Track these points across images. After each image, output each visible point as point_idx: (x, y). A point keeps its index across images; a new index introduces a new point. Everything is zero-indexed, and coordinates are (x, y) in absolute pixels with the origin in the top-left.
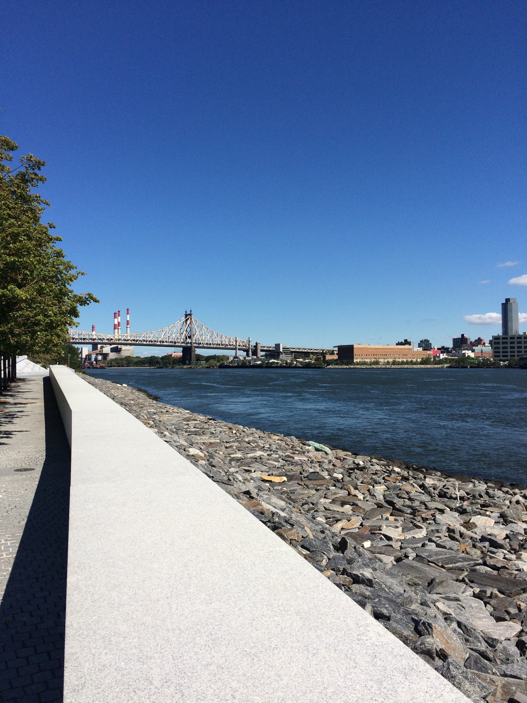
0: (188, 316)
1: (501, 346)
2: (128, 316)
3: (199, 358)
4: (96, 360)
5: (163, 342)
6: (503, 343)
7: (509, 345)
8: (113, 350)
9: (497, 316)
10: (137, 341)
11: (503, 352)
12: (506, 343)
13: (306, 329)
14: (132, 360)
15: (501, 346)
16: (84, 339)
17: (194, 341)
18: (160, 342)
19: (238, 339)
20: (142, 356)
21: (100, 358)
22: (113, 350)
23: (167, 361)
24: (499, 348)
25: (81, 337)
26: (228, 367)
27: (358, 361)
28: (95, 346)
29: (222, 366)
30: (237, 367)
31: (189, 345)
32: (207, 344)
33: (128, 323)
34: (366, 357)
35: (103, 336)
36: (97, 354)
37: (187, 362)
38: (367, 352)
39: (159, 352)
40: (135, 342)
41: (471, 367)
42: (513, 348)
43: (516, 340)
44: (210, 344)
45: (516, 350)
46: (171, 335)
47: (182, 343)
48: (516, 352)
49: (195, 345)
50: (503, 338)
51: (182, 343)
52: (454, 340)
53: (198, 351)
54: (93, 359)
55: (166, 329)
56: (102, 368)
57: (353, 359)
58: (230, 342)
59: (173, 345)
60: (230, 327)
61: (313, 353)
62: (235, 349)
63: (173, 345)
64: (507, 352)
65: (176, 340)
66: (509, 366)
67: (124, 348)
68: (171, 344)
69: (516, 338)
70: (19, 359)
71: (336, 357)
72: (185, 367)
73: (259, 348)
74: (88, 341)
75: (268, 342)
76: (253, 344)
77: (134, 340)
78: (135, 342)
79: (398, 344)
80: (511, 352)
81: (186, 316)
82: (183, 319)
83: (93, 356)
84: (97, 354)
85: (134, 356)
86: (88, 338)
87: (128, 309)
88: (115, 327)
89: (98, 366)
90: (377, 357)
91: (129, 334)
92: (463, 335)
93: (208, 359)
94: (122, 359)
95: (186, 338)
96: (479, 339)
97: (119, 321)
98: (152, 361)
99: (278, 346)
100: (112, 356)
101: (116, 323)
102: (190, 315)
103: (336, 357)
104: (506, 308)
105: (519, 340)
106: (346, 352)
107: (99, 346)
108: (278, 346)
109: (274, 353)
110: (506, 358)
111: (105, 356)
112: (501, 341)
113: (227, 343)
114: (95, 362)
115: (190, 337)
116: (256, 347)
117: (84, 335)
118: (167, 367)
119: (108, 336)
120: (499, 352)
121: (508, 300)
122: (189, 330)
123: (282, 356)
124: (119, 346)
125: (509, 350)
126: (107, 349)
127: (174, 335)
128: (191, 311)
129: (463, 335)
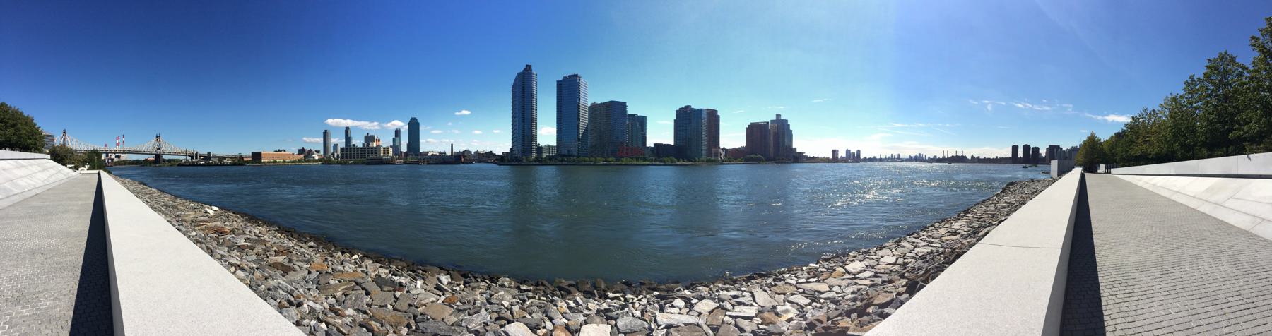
9: (321, 140)
39: (142, 157)
53: (164, 157)
60: (183, 141)
66: (354, 163)
70: (554, 143)
75: (203, 151)
91: (124, 148)
92: (778, 116)
93: (169, 161)
98: (137, 162)
104: (325, 134)
106: (257, 156)
109: (208, 157)
129: (778, 116)
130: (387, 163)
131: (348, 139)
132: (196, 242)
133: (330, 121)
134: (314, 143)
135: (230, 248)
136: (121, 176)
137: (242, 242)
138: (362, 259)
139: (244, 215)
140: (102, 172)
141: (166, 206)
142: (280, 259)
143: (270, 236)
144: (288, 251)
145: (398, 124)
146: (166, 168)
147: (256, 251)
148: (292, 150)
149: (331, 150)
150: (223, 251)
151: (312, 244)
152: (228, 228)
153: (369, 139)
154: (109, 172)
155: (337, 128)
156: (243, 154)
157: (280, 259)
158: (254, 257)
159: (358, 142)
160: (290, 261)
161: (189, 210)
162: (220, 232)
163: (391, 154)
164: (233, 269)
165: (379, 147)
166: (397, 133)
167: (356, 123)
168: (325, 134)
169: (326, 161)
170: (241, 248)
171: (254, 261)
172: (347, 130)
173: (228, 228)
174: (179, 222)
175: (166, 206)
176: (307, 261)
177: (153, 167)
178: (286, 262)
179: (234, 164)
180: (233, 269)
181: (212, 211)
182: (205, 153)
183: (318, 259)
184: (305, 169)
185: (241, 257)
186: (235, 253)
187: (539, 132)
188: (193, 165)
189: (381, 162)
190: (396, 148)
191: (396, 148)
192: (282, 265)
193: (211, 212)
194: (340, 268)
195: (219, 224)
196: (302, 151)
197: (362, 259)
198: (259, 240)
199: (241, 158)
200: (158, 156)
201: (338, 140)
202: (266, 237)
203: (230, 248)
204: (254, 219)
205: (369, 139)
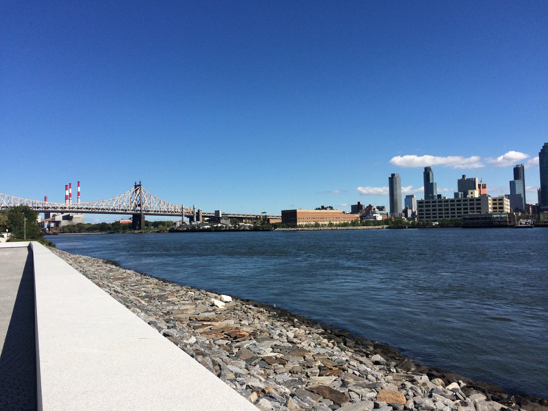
0: (137, 186)
1: (424, 209)
2: (79, 188)
3: (147, 224)
4: (49, 227)
5: (115, 210)
6: (426, 206)
7: (431, 208)
8: (65, 218)
9: (386, 190)
10: (90, 209)
11: (451, 213)
12: (429, 206)
13: (250, 195)
14: (84, 227)
15: (424, 209)
16: (38, 208)
17: (143, 209)
18: (112, 210)
19: (184, 207)
20: (93, 223)
21: (52, 225)
22: (65, 218)
23: (116, 228)
24: (422, 211)
25: (34, 205)
26: (177, 231)
27: (301, 223)
28: (47, 216)
29: (172, 231)
30: (188, 231)
31: (138, 212)
32: (155, 211)
33: (79, 194)
34: (307, 220)
35: (56, 205)
36: (49, 222)
37: (137, 227)
38: (308, 216)
39: (110, 219)
40: (88, 210)
41: (409, 228)
42: (435, 210)
43: (449, 203)
44: (158, 211)
45: (450, 211)
46: (122, 203)
47: (132, 210)
48: (450, 213)
49: (144, 212)
50: (426, 202)
51: (132, 210)
52: (352, 206)
53: (148, 218)
54: (46, 226)
55: (117, 198)
56: (55, 234)
57: (296, 222)
58: (175, 209)
59: (125, 212)
60: (178, 194)
61: (244, 218)
62: (182, 216)
63: (125, 212)
64: (430, 214)
65: (126, 208)
66: (441, 226)
67: (75, 215)
68: (122, 211)
69: (475, 200)
71: (280, 221)
72: (136, 232)
73: (201, 215)
74: (41, 209)
75: (208, 209)
76: (196, 211)
77: (87, 208)
78: (88, 210)
79: (317, 209)
80: (433, 214)
81: (136, 186)
82: (133, 189)
83: (46, 224)
84: (49, 222)
85: (86, 223)
86: (41, 206)
87: (78, 182)
88: (67, 198)
89: (51, 232)
90: (316, 220)
91: (80, 203)
92: (359, 203)
93: (156, 224)
94: (74, 226)
95: (136, 206)
96: (370, 205)
97: (71, 192)
98: (102, 227)
99: (217, 212)
100: (64, 223)
101: (67, 194)
102: (140, 185)
103: (280, 221)
104: (392, 181)
105: (471, 202)
106: (289, 217)
107: (51, 214)
108: (217, 212)
109: (215, 218)
110: (435, 219)
111: (57, 223)
112: (425, 204)
113: (173, 210)
114: (47, 229)
115: (139, 205)
116: (198, 213)
117: (38, 204)
118: (118, 232)
119: (60, 204)
120: (423, 214)
121: (393, 175)
122: (138, 199)
123: (222, 221)
124: (71, 214)
125: (431, 212)
126: (59, 217)
127: (124, 204)
128: (140, 182)
129: (359, 203)
130: (501, 224)
131: (429, 186)
132: (196, 354)
133: (397, 160)
134: (376, 195)
135: (250, 362)
136: (72, 251)
137: (268, 353)
138: (466, 390)
139: (269, 307)
140: (37, 245)
141: (150, 298)
142: (328, 381)
143: (311, 342)
144: (341, 368)
145: (516, 156)
146: (151, 236)
147: (289, 366)
148: (342, 207)
149: (402, 206)
150: (237, 367)
151: (378, 357)
152: (246, 330)
153: (466, 184)
154: (50, 245)
155: (409, 169)
156: (269, 214)
157: (328, 381)
158: (287, 377)
159: (447, 190)
160: (344, 384)
161: (184, 303)
162: (234, 336)
163: (507, 208)
164: (254, 396)
165: (483, 198)
166: (518, 172)
167: (440, 160)
168: (392, 181)
169: (394, 223)
170: (266, 362)
171: (286, 384)
172: (427, 172)
173: (246, 330)
174: (170, 326)
175: (150, 298)
176: (373, 387)
177: (130, 236)
178: (337, 386)
179: (255, 229)
180: (254, 396)
181: (222, 302)
182: (211, 211)
183: (389, 385)
184: (369, 238)
185: (267, 377)
186: (257, 370)
187: (24, 266)
188: (193, 230)
189: (488, 223)
190: (517, 199)
191: (517, 199)
192: (331, 391)
193: (220, 305)
194: (428, 402)
195: (232, 323)
196: (357, 208)
197: (466, 390)
198: (294, 348)
199: (266, 219)
200: (137, 218)
201: (413, 189)
202: (304, 344)
203: (250, 362)
204: (285, 315)
205: (466, 184)
